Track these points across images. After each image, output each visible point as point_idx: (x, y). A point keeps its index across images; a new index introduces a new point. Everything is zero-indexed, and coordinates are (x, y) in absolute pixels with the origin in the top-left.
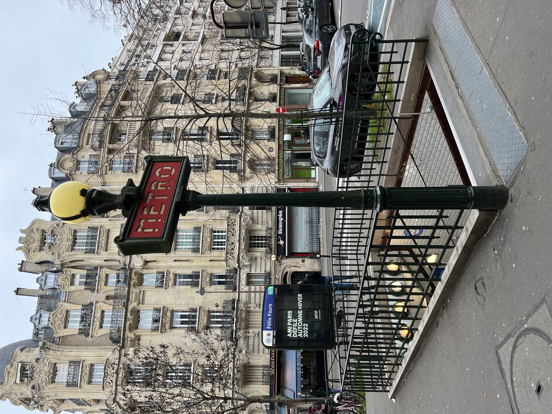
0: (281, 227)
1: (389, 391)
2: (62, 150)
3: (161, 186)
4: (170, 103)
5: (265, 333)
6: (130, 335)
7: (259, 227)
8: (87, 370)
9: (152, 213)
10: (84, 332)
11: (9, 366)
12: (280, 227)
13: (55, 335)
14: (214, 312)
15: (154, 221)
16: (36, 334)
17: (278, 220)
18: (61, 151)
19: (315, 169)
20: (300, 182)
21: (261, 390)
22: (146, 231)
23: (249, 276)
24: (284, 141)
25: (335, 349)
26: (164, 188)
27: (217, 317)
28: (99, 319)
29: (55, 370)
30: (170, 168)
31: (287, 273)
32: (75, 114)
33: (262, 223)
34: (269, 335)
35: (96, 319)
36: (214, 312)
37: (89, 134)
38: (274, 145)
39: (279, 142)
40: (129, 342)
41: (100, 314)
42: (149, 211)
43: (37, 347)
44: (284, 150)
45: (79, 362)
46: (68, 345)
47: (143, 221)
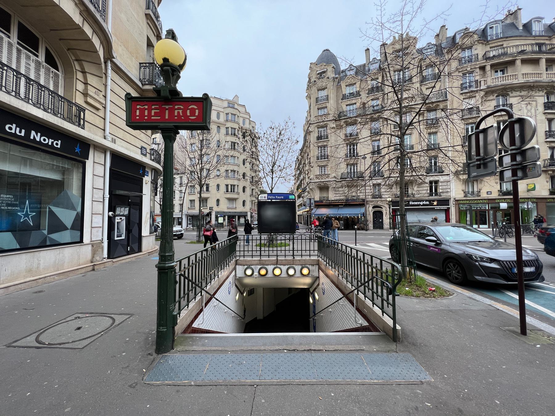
0: (415, 204)
2: (485, 31)
3: (178, 112)
4: (546, 101)
5: (266, 195)
6: (342, 123)
7: (416, 188)
8: (324, 106)
10: (344, 97)
11: (325, 64)
12: (415, 202)
13: (342, 82)
14: (357, 167)
16: (343, 72)
17: (421, 201)
18: (483, 30)
19: (489, 227)
20: (456, 216)
21: (317, 196)
23: (379, 185)
24: (499, 203)
25: (258, 233)
27: (354, 169)
28: (351, 103)
29: (324, 89)
30: (197, 114)
31: (382, 208)
32: (527, 27)
33: (419, 191)
34: (265, 197)
35: (351, 101)
36: (357, 167)
37: (502, 45)
38: (495, 195)
39: (498, 199)
40: (338, 123)
41: (354, 102)
43: (336, 75)
44: (488, 204)
45: (328, 100)
46: (337, 91)
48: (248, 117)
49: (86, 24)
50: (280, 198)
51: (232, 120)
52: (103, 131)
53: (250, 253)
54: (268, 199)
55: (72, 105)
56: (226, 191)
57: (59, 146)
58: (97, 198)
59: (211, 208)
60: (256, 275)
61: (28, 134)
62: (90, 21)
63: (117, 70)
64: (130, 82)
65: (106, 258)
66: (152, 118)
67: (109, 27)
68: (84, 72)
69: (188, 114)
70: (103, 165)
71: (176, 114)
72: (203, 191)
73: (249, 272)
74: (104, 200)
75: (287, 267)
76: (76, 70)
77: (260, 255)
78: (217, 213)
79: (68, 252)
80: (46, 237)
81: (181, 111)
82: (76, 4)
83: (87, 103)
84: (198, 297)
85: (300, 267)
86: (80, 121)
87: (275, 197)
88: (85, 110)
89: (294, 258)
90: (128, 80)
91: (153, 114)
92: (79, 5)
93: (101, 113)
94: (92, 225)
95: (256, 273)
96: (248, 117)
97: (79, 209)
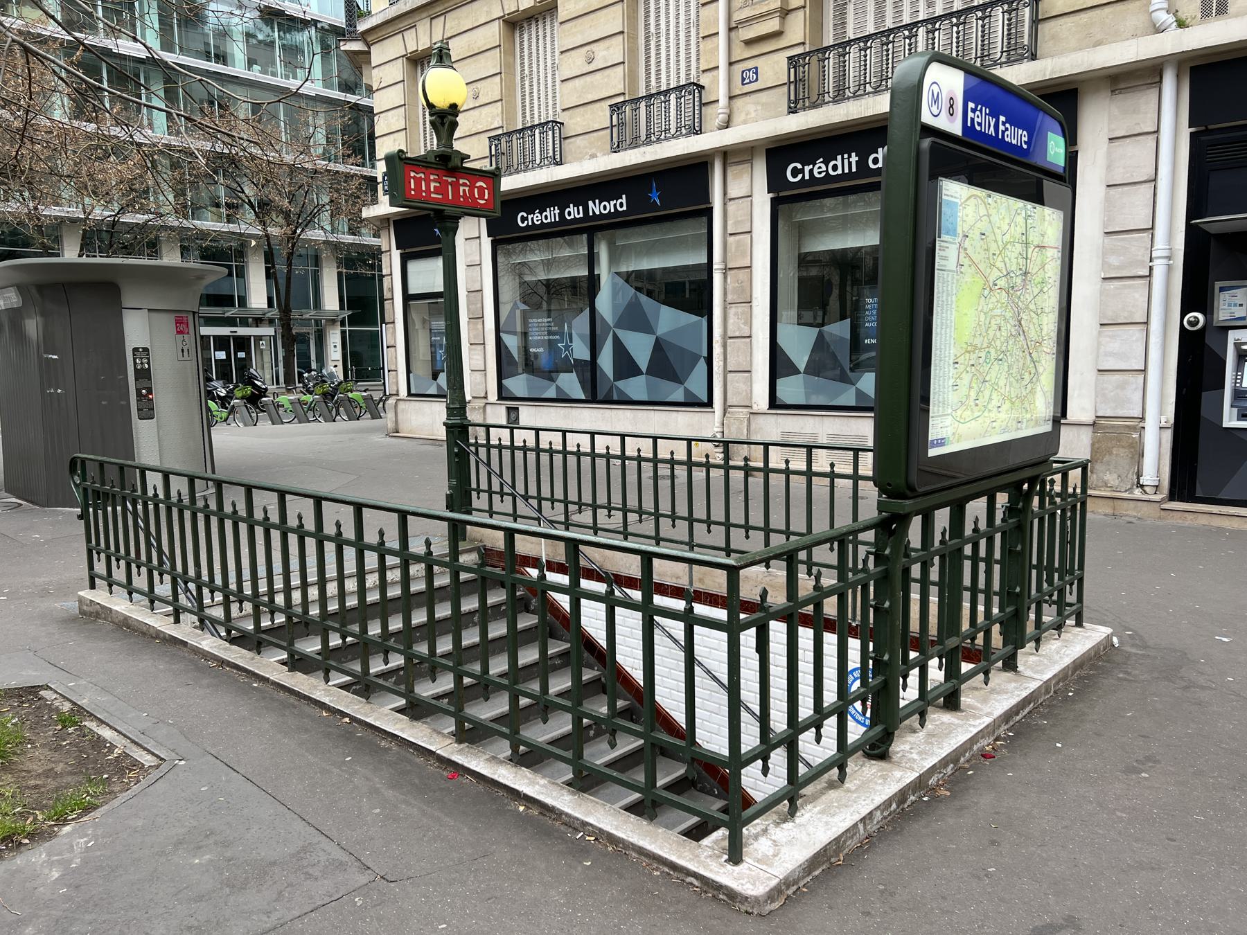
1: (93, 586)
3: (464, 191)
9: (432, 185)
15: (424, 188)
22: (412, 181)
26: (461, 194)
30: (486, 197)
42: (435, 180)
47: (423, 177)
53: (648, 527)
58: (1118, 268)
80: (611, 388)
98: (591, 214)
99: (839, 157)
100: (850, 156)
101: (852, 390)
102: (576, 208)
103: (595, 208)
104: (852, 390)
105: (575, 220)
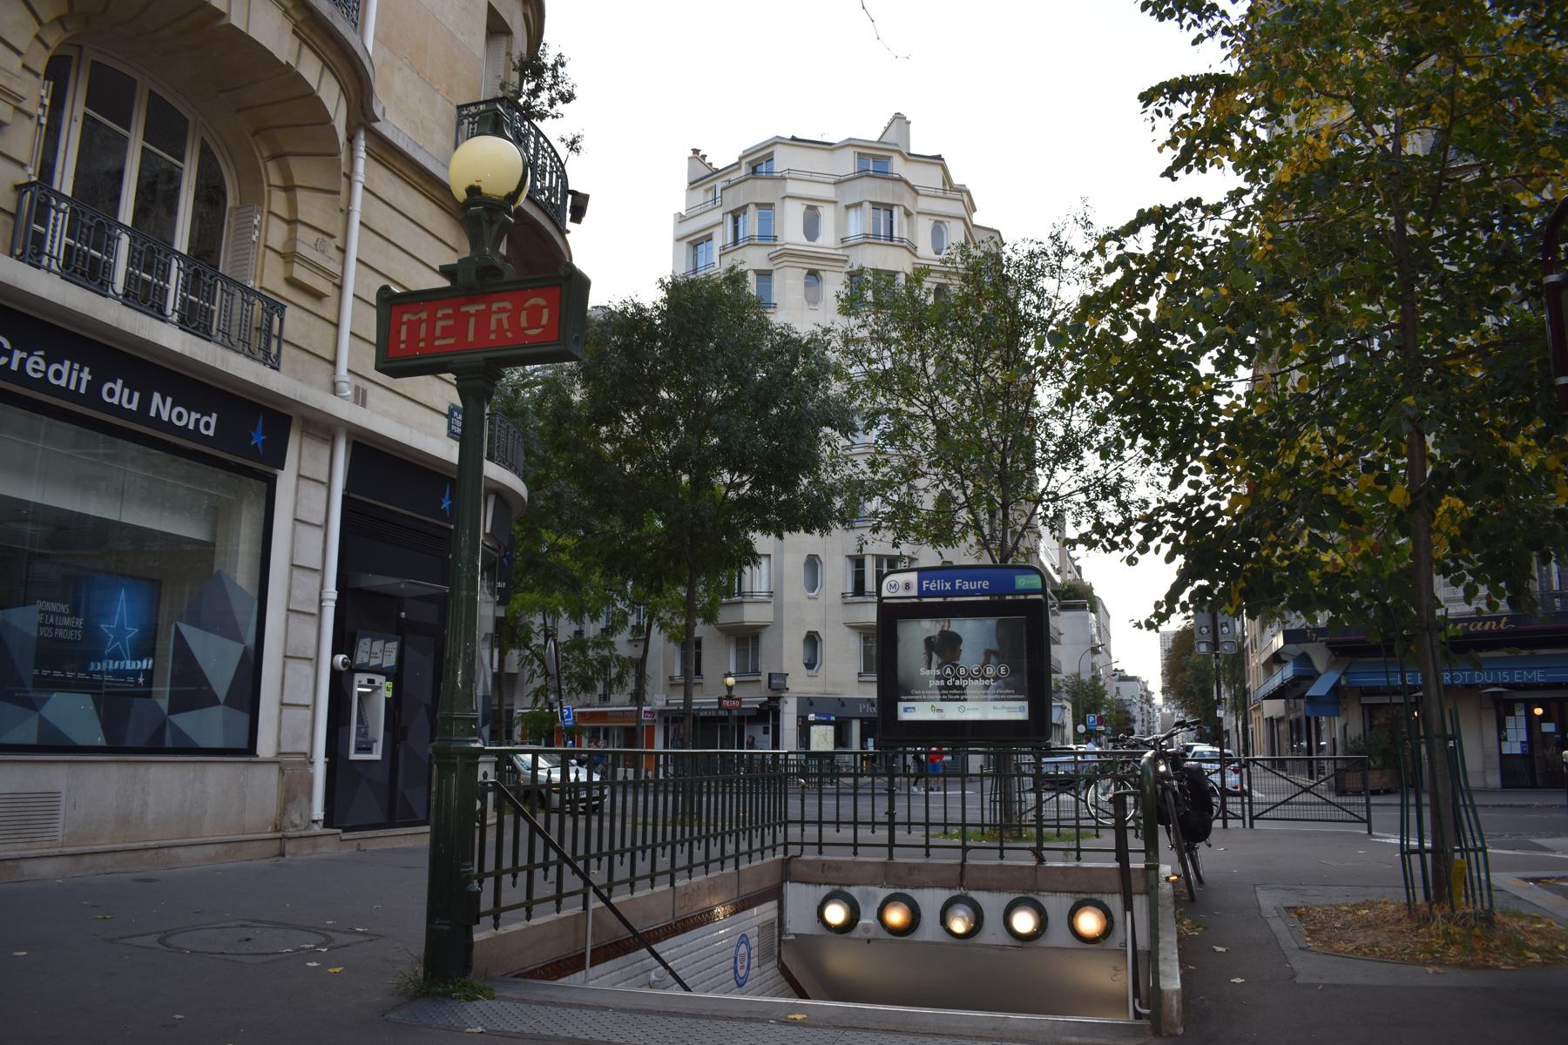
3: (499, 321)
5: (913, 577)
30: (544, 321)
48: (957, 209)
49: (308, 55)
50: (973, 586)
51: (877, 236)
52: (329, 367)
54: (922, 594)
55: (252, 298)
56: (850, 588)
57: (211, 433)
59: (777, 684)
60: (866, 929)
61: (145, 403)
62: (318, 42)
63: (388, 154)
64: (421, 182)
65: (321, 824)
66: (437, 343)
67: (369, 41)
68: (289, 188)
69: (524, 322)
70: (323, 483)
71: (493, 326)
72: (740, 593)
73: (836, 914)
74: (321, 608)
75: (1007, 898)
76: (269, 185)
77: (891, 844)
78: (806, 704)
79: (216, 777)
81: (504, 316)
82: (286, 12)
83: (292, 282)
84: (571, 909)
85: (1067, 901)
86: (268, 344)
87: (953, 586)
88: (284, 307)
89: (1041, 860)
90: (416, 178)
91: (438, 332)
92: (292, 12)
93: (328, 310)
94: (282, 695)
95: (867, 919)
96: (963, 212)
97: (250, 640)
98: (153, 414)
99: (67, 363)
100: (81, 370)
101: (33, 721)
102: (126, 391)
103: (162, 407)
104: (33, 721)
105: (118, 410)
